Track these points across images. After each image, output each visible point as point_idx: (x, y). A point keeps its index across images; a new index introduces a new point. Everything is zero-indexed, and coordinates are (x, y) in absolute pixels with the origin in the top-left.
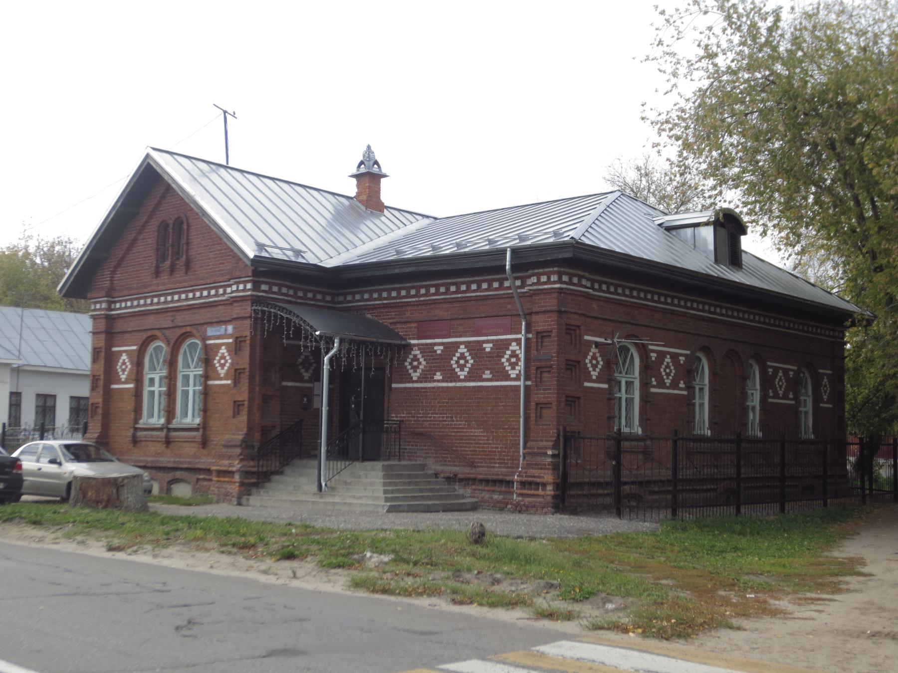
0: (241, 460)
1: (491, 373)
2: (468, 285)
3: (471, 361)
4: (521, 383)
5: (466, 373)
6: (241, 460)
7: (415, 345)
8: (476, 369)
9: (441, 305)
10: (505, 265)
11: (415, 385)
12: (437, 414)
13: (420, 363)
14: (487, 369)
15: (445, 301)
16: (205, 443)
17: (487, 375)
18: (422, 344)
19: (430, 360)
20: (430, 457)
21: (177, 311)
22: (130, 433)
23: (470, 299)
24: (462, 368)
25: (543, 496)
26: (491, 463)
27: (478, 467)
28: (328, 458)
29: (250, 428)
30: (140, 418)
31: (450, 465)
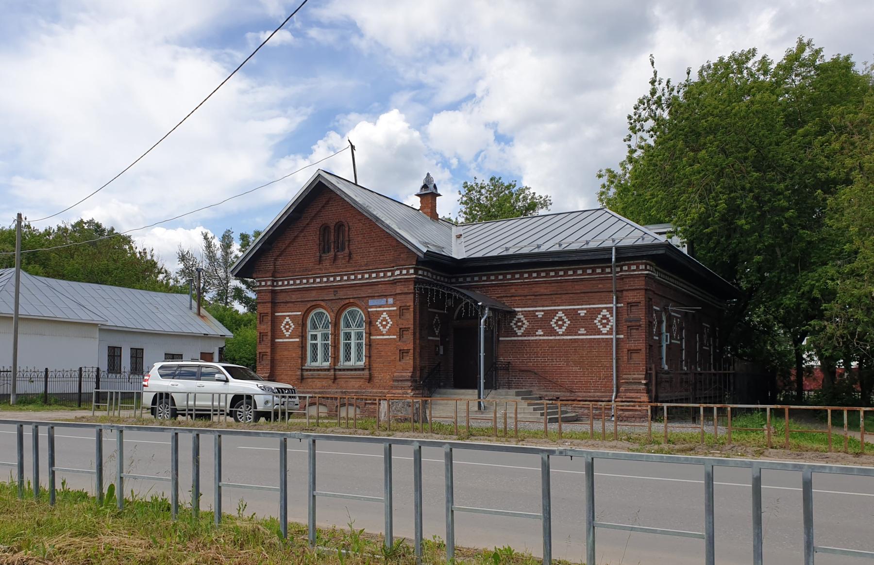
0: (412, 390)
1: (585, 330)
2: (530, 273)
3: (293, 326)
4: (613, 336)
5: (564, 330)
6: (412, 390)
7: (519, 312)
8: (572, 327)
9: (542, 285)
10: (612, 258)
11: (520, 338)
12: (540, 357)
13: (284, 327)
14: (582, 327)
15: (545, 282)
16: (370, 379)
17: (582, 331)
18: (525, 311)
19: (532, 321)
20: (535, 386)
21: (339, 288)
22: (299, 373)
23: (567, 281)
24: (287, 330)
25: (640, 411)
26: (587, 389)
27: (575, 392)
28: (485, 388)
29: (414, 368)
30: (306, 363)
31: (552, 391)
